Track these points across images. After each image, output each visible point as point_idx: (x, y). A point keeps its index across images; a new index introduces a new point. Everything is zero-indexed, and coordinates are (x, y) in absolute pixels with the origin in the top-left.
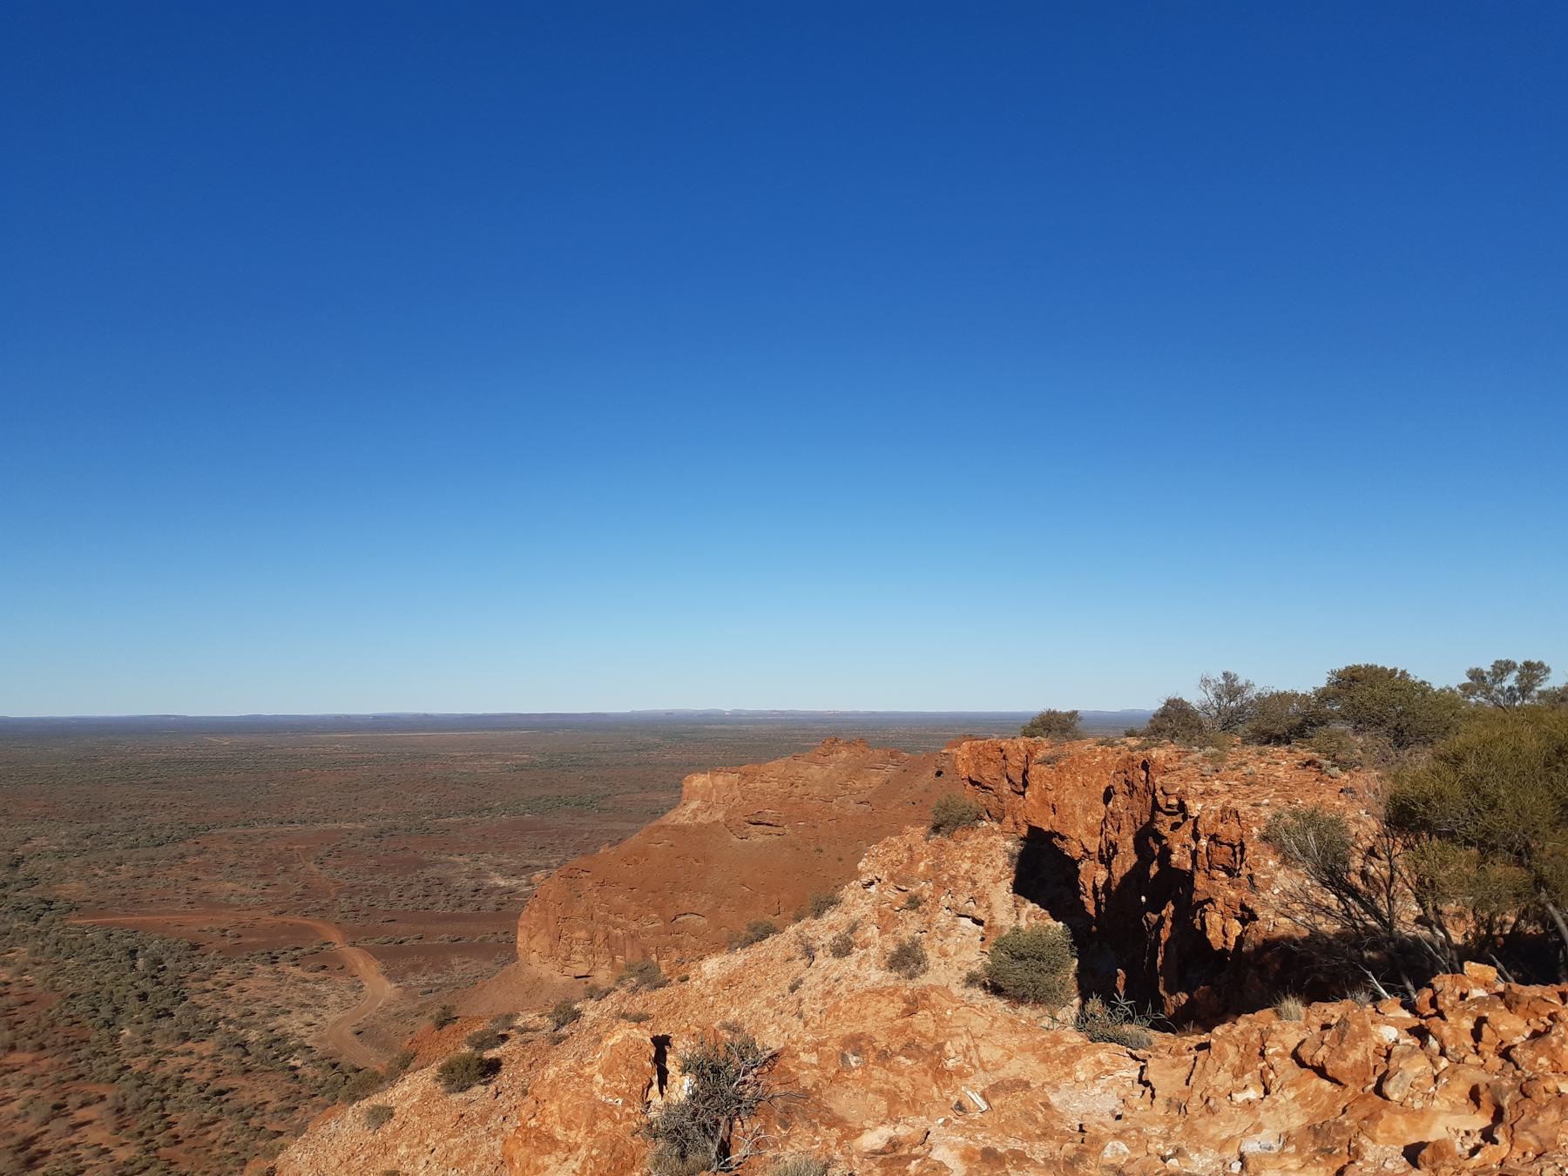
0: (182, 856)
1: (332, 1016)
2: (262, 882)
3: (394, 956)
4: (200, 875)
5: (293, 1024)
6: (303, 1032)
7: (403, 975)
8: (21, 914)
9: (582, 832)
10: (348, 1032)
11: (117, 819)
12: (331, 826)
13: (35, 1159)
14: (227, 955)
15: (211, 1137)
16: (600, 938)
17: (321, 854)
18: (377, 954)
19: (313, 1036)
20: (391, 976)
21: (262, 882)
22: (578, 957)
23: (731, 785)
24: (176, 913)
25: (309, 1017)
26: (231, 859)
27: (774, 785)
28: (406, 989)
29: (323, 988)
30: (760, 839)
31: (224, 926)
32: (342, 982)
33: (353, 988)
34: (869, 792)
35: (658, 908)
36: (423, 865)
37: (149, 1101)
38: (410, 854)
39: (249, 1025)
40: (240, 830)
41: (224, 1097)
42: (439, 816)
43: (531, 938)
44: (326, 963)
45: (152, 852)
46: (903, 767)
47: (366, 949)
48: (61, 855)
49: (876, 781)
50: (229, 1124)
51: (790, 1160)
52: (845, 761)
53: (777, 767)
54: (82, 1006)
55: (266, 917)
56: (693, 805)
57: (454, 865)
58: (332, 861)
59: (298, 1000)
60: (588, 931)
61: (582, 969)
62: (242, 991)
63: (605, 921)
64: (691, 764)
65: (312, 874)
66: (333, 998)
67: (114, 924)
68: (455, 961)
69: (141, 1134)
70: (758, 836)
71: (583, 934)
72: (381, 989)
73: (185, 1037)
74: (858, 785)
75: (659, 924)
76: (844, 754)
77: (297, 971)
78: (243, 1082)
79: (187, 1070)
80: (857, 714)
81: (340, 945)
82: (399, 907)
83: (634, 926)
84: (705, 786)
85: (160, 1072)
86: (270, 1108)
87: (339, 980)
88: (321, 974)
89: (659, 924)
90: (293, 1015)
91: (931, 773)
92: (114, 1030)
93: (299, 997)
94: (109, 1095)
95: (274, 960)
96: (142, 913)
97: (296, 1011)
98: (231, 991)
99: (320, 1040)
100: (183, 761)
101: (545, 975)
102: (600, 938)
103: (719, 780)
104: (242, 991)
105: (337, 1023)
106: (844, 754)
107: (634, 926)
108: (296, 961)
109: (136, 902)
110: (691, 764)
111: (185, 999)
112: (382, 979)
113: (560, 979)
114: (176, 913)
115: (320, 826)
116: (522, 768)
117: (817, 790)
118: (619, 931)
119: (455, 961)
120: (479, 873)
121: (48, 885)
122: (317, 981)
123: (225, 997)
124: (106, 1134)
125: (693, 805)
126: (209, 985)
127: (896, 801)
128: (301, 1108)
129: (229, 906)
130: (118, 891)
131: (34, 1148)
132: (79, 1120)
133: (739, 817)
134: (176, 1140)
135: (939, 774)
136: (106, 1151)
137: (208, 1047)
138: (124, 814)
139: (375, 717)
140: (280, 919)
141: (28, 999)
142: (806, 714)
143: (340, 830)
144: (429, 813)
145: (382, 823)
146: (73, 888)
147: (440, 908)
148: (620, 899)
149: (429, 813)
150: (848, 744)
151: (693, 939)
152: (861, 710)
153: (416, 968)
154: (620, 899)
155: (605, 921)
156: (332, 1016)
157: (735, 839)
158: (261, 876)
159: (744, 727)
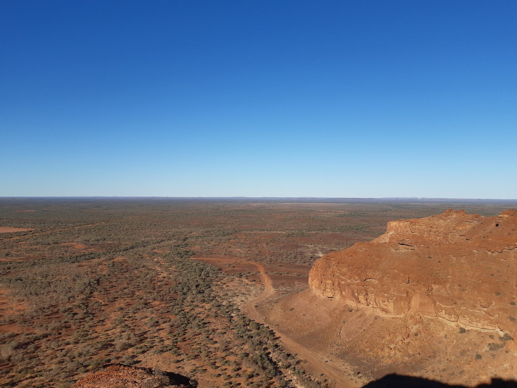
0: (230, 239)
1: (251, 299)
2: (248, 249)
3: (278, 279)
4: (232, 246)
5: (237, 300)
6: (239, 304)
7: (278, 287)
8: (179, 255)
9: (354, 239)
10: (254, 305)
11: (217, 227)
12: (272, 232)
13: (143, 340)
14: (228, 273)
15: (196, 340)
16: (336, 284)
17: (268, 241)
18: (272, 278)
19: (242, 306)
20: (274, 286)
21: (248, 249)
22: (328, 290)
23: (406, 226)
24: (220, 258)
25: (243, 298)
26: (242, 241)
27: (424, 227)
28: (278, 291)
29: (252, 288)
30: (403, 251)
31: (231, 263)
32: (259, 286)
33: (261, 289)
34: (465, 232)
35: (359, 275)
36: (298, 247)
37: (182, 324)
38: (295, 243)
39: (224, 299)
40: (249, 232)
41: (206, 325)
42: (309, 231)
43: (312, 280)
44: (256, 279)
45: (221, 238)
46: (481, 222)
47: (269, 275)
48: (197, 238)
49: (468, 227)
50: (203, 336)
51: (480, 325)
52: (455, 219)
53: (425, 220)
54: (180, 287)
55: (244, 261)
56: (391, 233)
57: (308, 248)
58: (271, 244)
59: (242, 292)
60: (332, 280)
61: (330, 295)
62: (227, 286)
63: (338, 277)
64: (401, 217)
65: (263, 247)
66: (254, 292)
67: (200, 260)
68: (296, 283)
69: (175, 336)
70: (403, 249)
71: (330, 282)
72: (270, 290)
73: (204, 301)
74: (460, 228)
75: (359, 281)
76: (455, 216)
77: (247, 281)
78: (214, 320)
79: (199, 314)
80: (472, 200)
81: (262, 273)
82: (285, 261)
83: (349, 281)
84: (396, 226)
85: (193, 312)
86: (218, 331)
87: (258, 285)
88: (253, 283)
89: (359, 281)
90: (239, 297)
91: (494, 225)
92: (186, 296)
93: (243, 290)
94: (173, 319)
95: (241, 276)
96: (211, 257)
97: (240, 295)
98: (224, 286)
99: (244, 307)
100: (241, 210)
101: (317, 295)
102: (336, 284)
103: (401, 224)
104: (227, 286)
105: (251, 302)
106: (455, 216)
107: (349, 281)
108: (247, 277)
109: (211, 253)
110: (401, 217)
111: (210, 287)
112: (272, 286)
113: (322, 297)
114: (220, 258)
115: (272, 232)
116: (340, 216)
117: (442, 230)
118: (343, 282)
119: (296, 283)
120: (315, 251)
121: (190, 247)
122: (251, 285)
123: (222, 288)
124: (165, 334)
125: (391, 233)
126: (219, 283)
127: (477, 236)
128: (227, 333)
129: (236, 256)
130: (208, 249)
131: (145, 336)
132: (161, 328)
133: (395, 241)
134: (184, 340)
135: (497, 225)
136: (163, 341)
137: (207, 306)
138: (219, 225)
139: (299, 198)
140: (248, 262)
141: (168, 283)
142: (451, 199)
143: (277, 234)
144: (306, 229)
145: (290, 232)
146: (197, 248)
147: (297, 263)
148: (344, 270)
149: (306, 229)
150: (457, 212)
151: (372, 289)
152: (474, 198)
153: (283, 284)
154: (344, 270)
155: (338, 277)
156: (251, 299)
157: (393, 250)
158: (248, 247)
159: (425, 204)
